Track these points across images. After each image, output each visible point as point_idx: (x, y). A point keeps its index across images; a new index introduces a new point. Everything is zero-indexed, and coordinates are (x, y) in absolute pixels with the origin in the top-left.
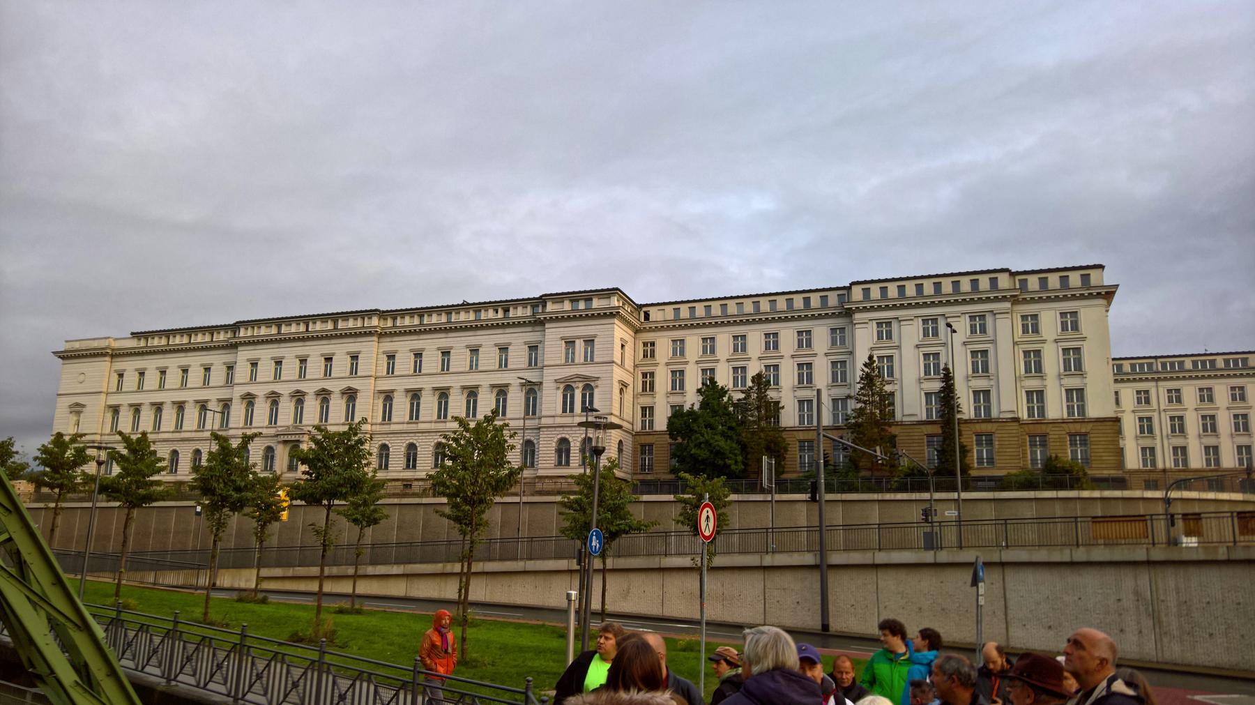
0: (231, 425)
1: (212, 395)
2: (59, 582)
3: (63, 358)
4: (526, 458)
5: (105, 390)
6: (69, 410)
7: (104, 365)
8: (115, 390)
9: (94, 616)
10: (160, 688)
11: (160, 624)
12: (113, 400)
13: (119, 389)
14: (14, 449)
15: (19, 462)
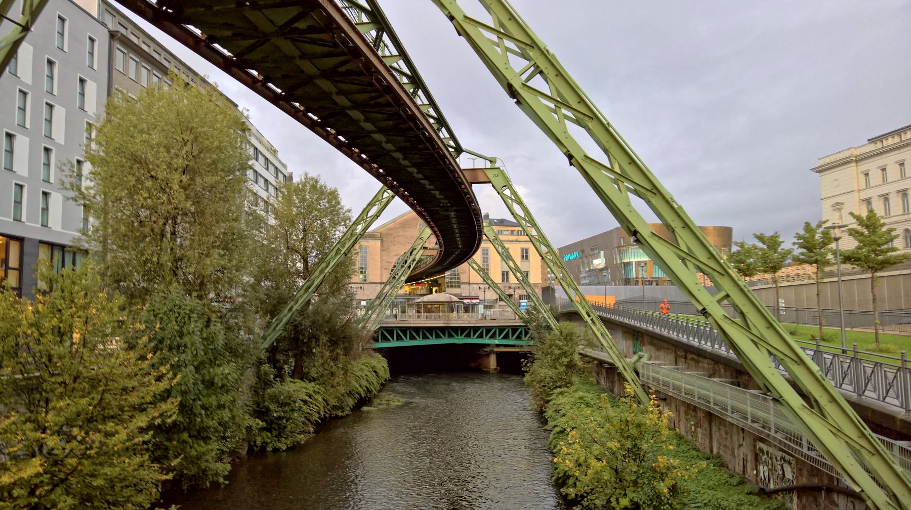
2: (771, 326)
3: (819, 172)
5: (856, 188)
6: (832, 209)
7: (852, 169)
8: (864, 187)
9: (803, 348)
10: (900, 417)
12: (865, 195)
13: (868, 186)
14: (780, 240)
15: (786, 249)
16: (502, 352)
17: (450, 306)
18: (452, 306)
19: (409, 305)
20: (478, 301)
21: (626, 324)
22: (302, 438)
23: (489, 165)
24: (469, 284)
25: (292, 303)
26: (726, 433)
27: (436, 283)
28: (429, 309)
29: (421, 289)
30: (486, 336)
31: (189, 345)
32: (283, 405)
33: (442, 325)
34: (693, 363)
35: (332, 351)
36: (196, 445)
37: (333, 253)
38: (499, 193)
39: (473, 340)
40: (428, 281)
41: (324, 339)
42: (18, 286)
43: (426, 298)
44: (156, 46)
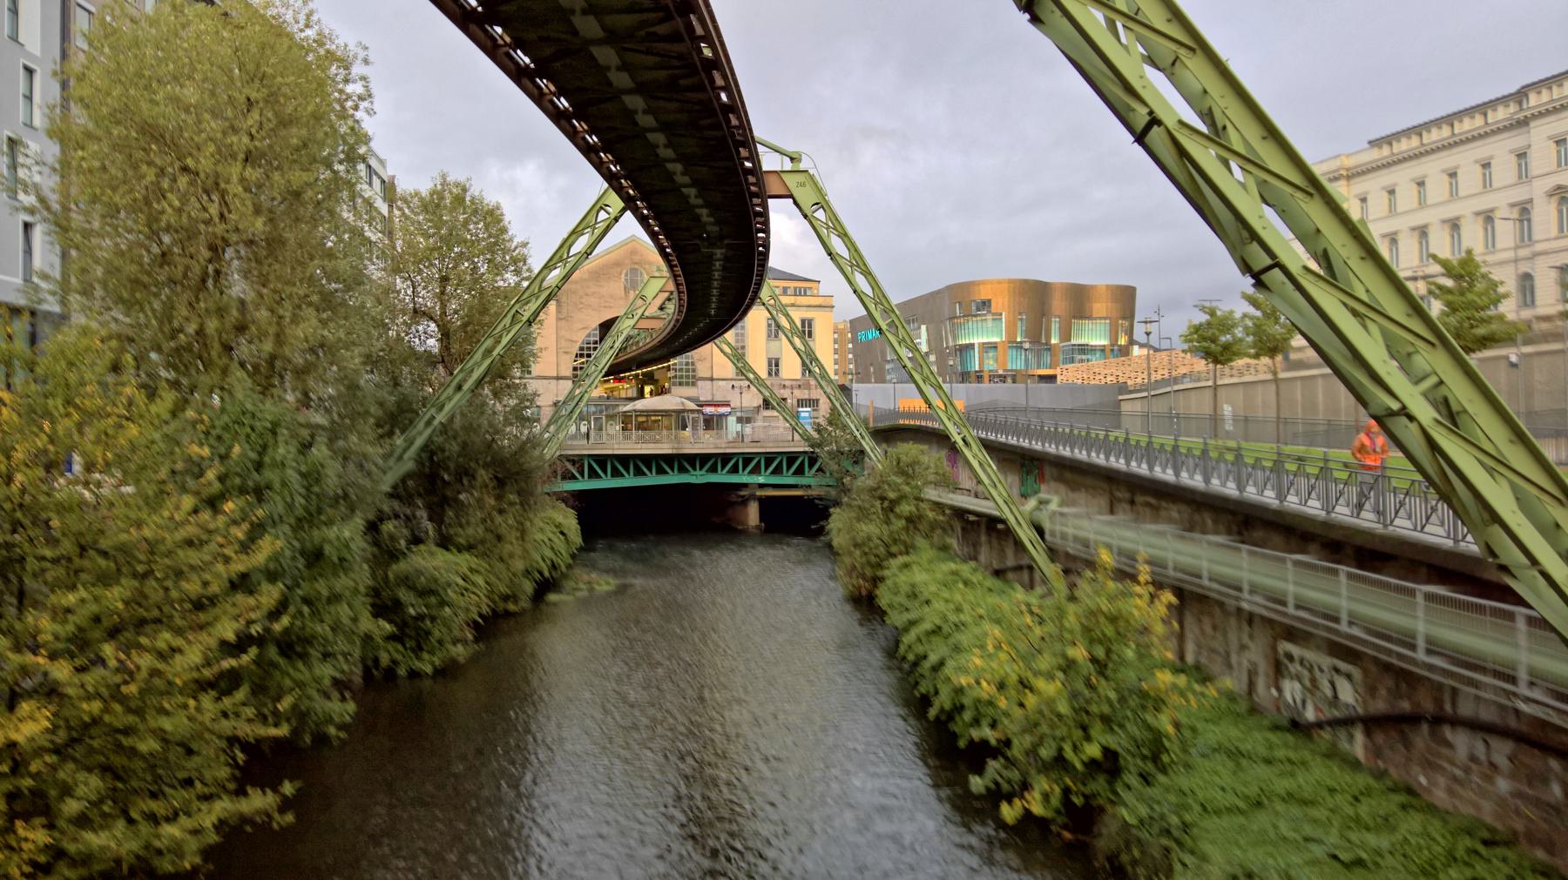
0: (1536, 237)
1: (1500, 201)
4: (1525, 296)
10: (1320, 519)
11: (1403, 475)
16: (768, 498)
17: (680, 419)
18: (684, 419)
19: (607, 416)
20: (728, 409)
21: (1012, 446)
22: (460, 652)
23: (788, 166)
24: (712, 379)
25: (433, 411)
26: (1215, 628)
27: (650, 378)
28: (646, 422)
29: (627, 389)
30: (744, 469)
31: (277, 486)
32: (424, 593)
33: (670, 452)
34: (1148, 510)
35: (499, 498)
36: (291, 671)
37: (507, 321)
38: (805, 216)
39: (722, 477)
40: (637, 375)
41: (483, 475)
43: (640, 405)
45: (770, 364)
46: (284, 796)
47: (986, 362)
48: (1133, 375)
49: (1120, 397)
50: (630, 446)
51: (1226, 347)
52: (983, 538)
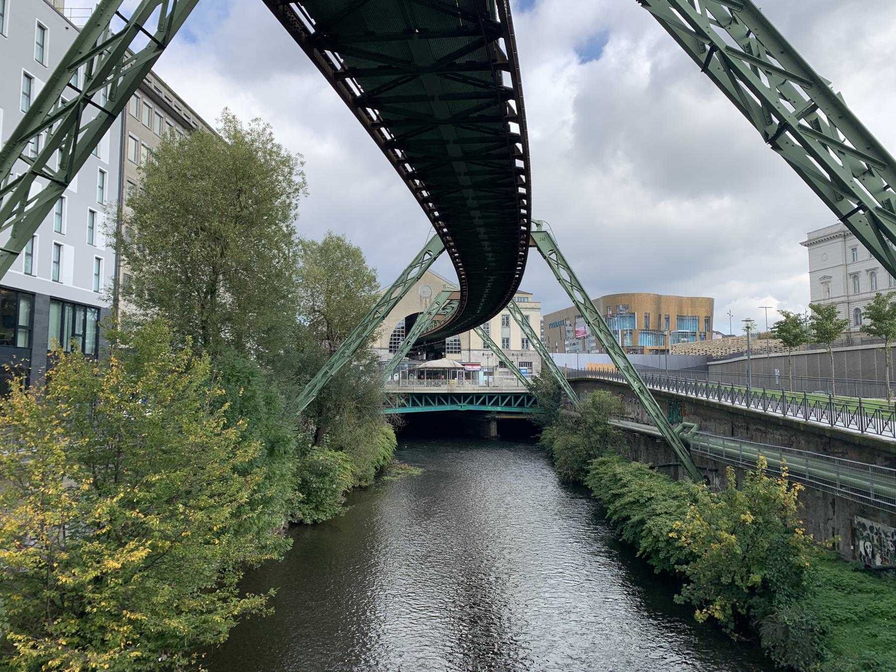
16: (502, 419)
20: (480, 367)
28: (434, 374)
33: (446, 392)
34: (759, 434)
38: (545, 258)
42: (27, 346)
44: (167, 92)
45: (503, 341)
46: (271, 596)
47: (625, 341)
48: (716, 350)
49: (708, 363)
50: (421, 388)
51: (796, 336)
52: (642, 447)
